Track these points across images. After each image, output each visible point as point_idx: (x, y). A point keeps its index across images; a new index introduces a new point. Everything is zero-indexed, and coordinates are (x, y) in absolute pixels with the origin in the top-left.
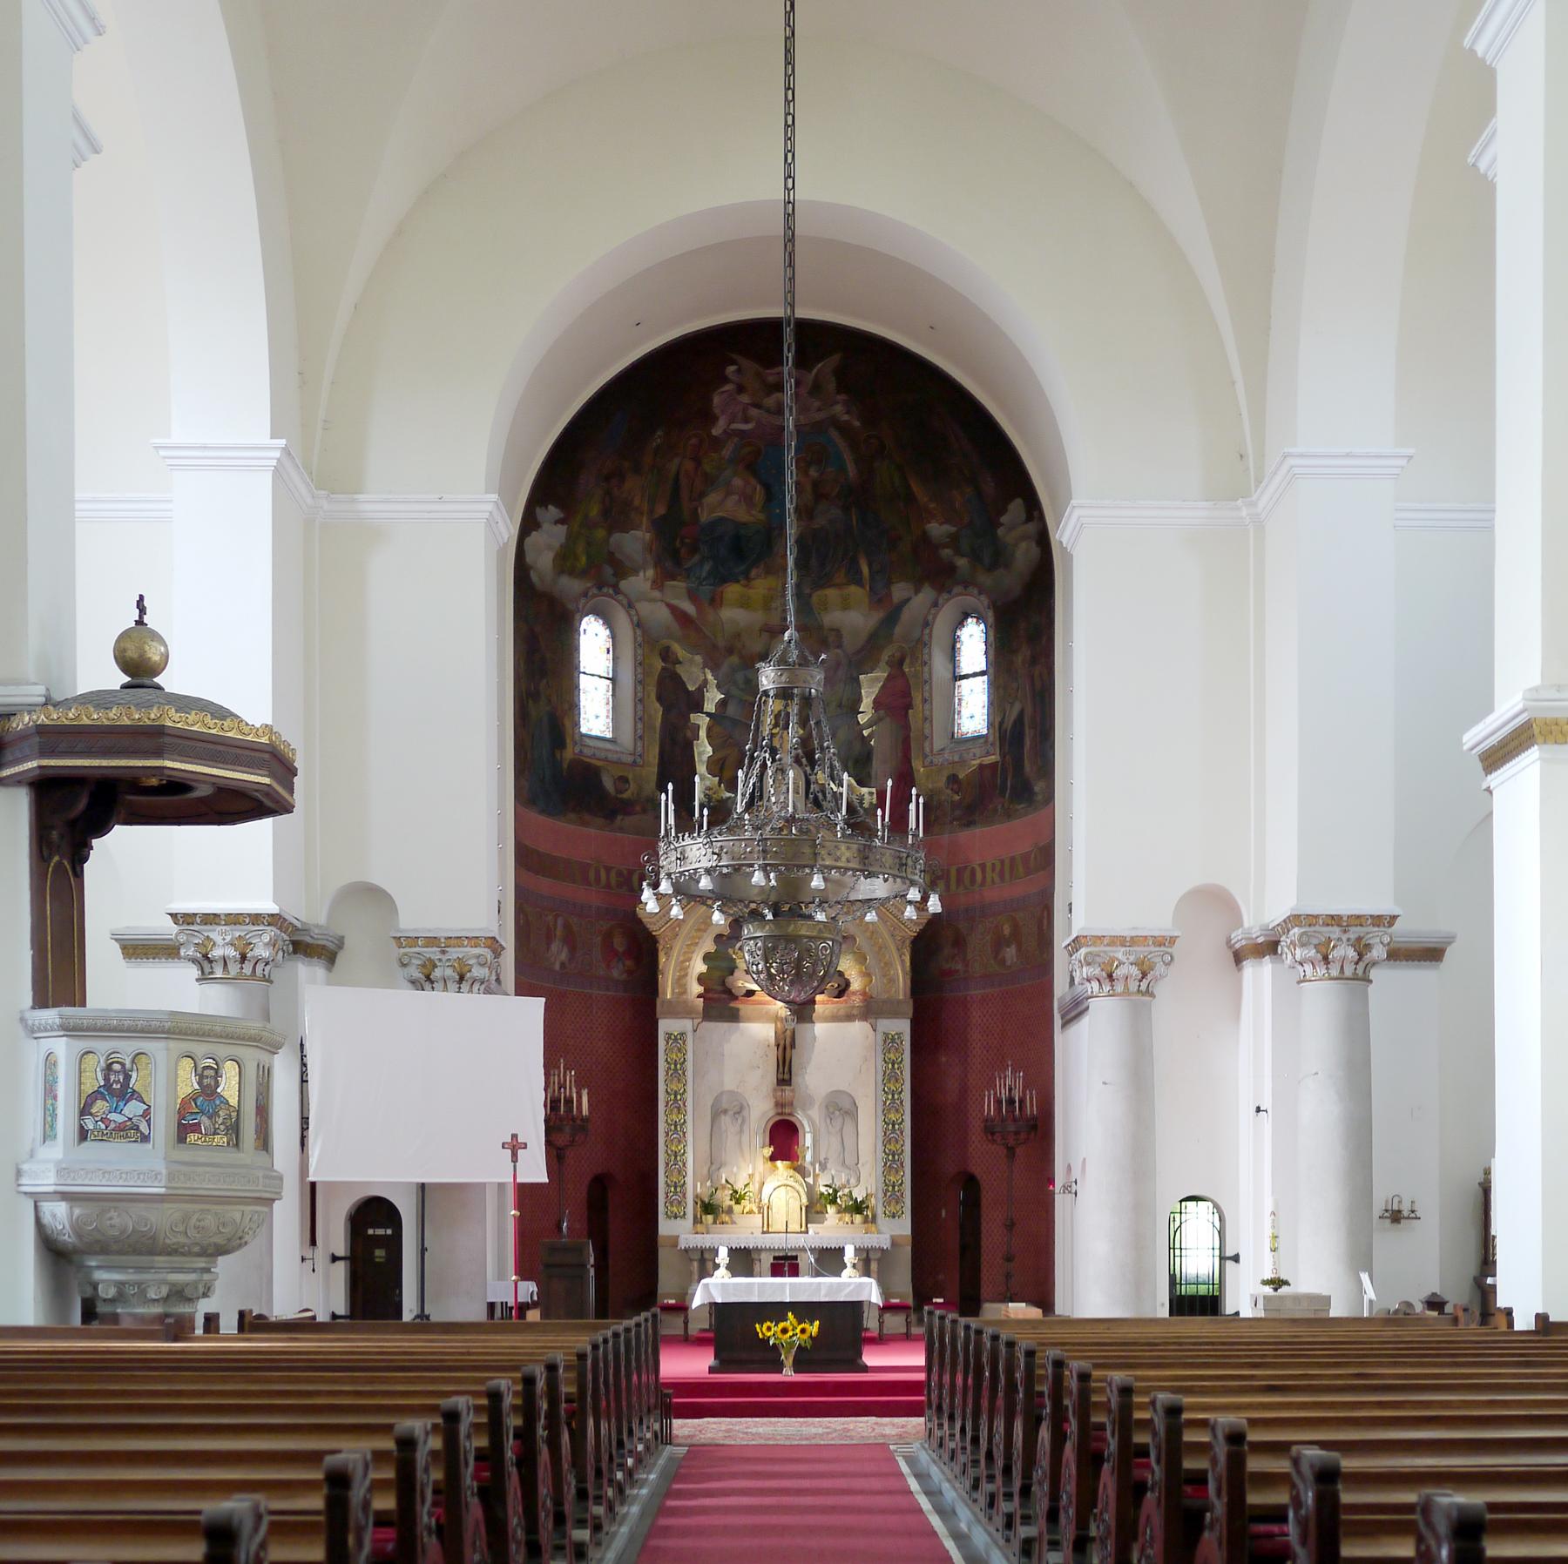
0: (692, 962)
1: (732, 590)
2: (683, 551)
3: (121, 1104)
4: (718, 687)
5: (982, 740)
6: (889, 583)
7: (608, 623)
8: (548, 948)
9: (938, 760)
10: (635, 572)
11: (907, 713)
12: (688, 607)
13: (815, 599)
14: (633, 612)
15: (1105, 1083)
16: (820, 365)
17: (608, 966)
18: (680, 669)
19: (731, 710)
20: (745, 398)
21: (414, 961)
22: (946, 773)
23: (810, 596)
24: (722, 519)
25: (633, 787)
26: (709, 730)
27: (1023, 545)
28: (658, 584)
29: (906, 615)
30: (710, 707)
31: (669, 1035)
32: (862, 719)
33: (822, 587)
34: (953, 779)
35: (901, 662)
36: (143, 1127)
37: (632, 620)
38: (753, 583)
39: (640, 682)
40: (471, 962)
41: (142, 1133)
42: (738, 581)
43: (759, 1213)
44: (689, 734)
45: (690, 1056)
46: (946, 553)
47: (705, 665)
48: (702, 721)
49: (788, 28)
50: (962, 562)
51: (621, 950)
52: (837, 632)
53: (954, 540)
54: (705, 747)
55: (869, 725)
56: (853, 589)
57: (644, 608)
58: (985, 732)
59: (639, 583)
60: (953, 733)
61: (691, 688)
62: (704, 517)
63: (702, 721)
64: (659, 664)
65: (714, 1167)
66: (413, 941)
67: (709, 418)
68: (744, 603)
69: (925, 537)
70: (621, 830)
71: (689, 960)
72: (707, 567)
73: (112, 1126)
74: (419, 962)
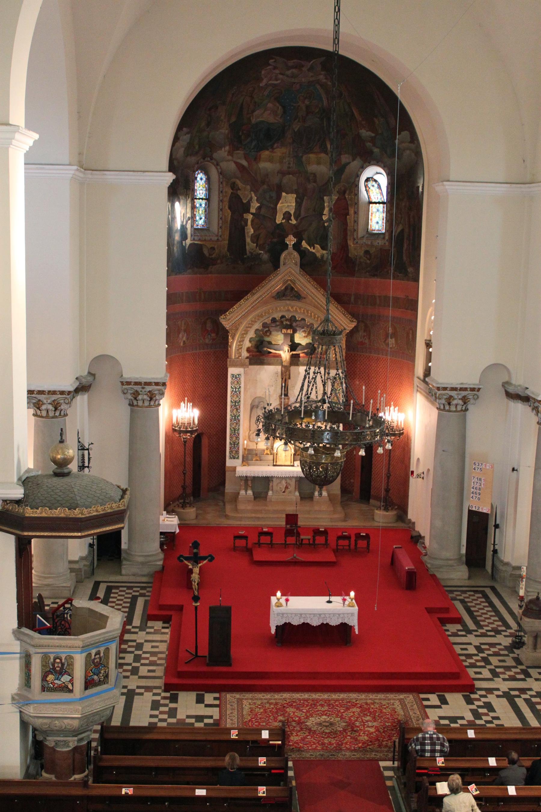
0: (244, 342)
1: (265, 154)
2: (243, 137)
3: (60, 676)
4: (257, 200)
5: (382, 236)
6: (340, 154)
7: (206, 173)
8: (178, 336)
9: (360, 242)
10: (221, 148)
11: (346, 217)
12: (245, 163)
13: (304, 158)
14: (219, 167)
15: (444, 451)
16: (314, 61)
17: (204, 338)
18: (239, 193)
19: (263, 211)
20: (277, 71)
21: (129, 391)
22: (364, 249)
23: (302, 157)
24: (262, 122)
25: (217, 251)
26: (252, 221)
27: (408, 152)
28: (230, 153)
29: (347, 170)
30: (253, 210)
31: (233, 375)
32: (325, 218)
33: (308, 153)
34: (367, 252)
35: (344, 192)
36: (70, 686)
37: (218, 171)
38: (275, 150)
39: (221, 201)
40: (156, 392)
41: (69, 689)
42: (268, 150)
43: (271, 454)
44: (243, 223)
45: (242, 385)
46: (369, 144)
47: (251, 190)
48: (250, 217)
49: (336, 20)
50: (376, 150)
51: (209, 329)
52: (315, 175)
53: (373, 140)
54: (250, 229)
55: (329, 220)
56: (323, 155)
57: (224, 165)
58: (384, 231)
59: (222, 153)
60: (368, 229)
61: (245, 202)
62: (253, 121)
63: (250, 217)
64: (230, 191)
65: (251, 432)
66: (129, 383)
67: (260, 79)
68: (271, 160)
69: (359, 136)
70: (211, 273)
71: (243, 341)
72: (254, 143)
73: (56, 685)
74: (132, 392)
